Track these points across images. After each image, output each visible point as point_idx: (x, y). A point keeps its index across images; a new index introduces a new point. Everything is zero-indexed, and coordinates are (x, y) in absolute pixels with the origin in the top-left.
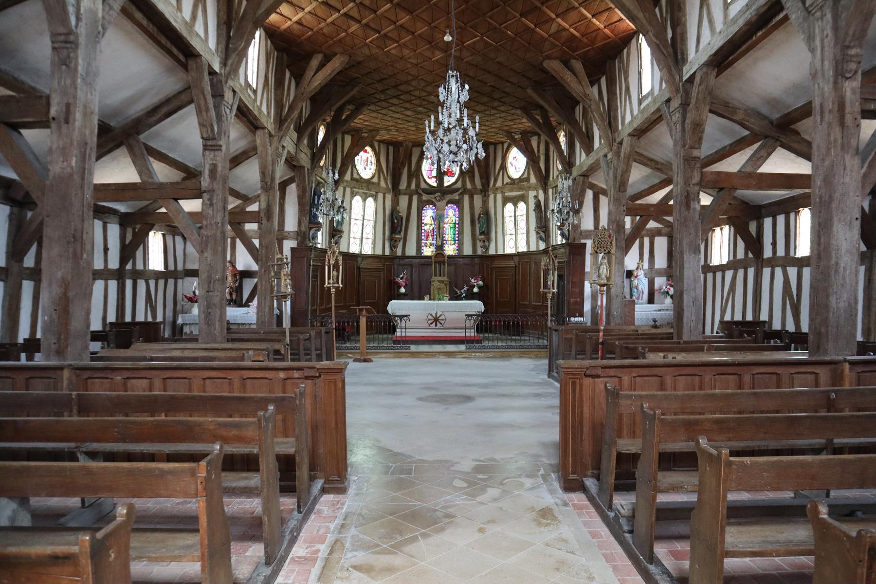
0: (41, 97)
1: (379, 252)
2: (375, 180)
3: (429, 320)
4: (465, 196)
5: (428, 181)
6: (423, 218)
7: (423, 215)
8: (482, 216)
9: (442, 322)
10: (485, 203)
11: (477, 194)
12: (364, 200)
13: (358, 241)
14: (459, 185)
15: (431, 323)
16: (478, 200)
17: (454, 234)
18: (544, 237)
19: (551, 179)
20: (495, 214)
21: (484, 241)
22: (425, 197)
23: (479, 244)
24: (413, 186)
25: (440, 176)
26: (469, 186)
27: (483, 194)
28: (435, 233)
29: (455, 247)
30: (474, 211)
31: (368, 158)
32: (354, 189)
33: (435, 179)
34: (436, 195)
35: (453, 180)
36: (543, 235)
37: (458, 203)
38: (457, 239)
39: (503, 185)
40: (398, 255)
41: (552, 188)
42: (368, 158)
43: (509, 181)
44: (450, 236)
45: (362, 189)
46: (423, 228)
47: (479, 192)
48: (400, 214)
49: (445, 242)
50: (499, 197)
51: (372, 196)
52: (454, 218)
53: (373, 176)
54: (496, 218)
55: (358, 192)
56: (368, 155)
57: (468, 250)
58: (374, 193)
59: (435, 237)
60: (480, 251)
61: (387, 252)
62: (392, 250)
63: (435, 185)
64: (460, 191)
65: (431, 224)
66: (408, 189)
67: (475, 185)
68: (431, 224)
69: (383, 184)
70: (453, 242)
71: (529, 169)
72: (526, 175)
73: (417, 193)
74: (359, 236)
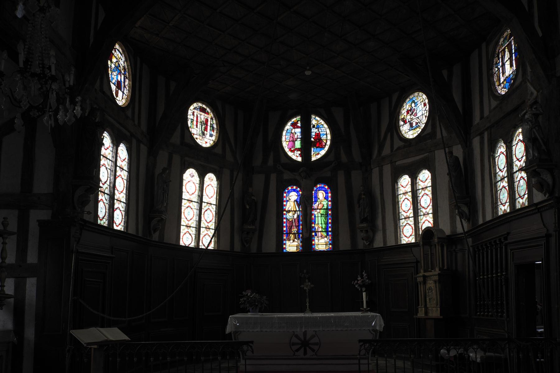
2: (219, 150)
3: (294, 344)
5: (290, 154)
6: (285, 203)
7: (285, 199)
8: (363, 196)
9: (316, 347)
12: (202, 177)
13: (193, 231)
15: (298, 350)
16: (357, 177)
19: (477, 119)
20: (382, 193)
22: (287, 176)
23: (360, 235)
24: (271, 162)
25: (305, 151)
26: (344, 158)
28: (301, 223)
33: (299, 152)
34: (301, 170)
35: (323, 152)
36: (465, 209)
39: (392, 151)
41: (481, 134)
42: (207, 120)
43: (401, 144)
46: (285, 216)
48: (253, 197)
50: (387, 169)
57: (345, 244)
59: (301, 227)
60: (361, 244)
61: (238, 247)
63: (299, 159)
65: (295, 211)
70: (325, 234)
74: (193, 224)
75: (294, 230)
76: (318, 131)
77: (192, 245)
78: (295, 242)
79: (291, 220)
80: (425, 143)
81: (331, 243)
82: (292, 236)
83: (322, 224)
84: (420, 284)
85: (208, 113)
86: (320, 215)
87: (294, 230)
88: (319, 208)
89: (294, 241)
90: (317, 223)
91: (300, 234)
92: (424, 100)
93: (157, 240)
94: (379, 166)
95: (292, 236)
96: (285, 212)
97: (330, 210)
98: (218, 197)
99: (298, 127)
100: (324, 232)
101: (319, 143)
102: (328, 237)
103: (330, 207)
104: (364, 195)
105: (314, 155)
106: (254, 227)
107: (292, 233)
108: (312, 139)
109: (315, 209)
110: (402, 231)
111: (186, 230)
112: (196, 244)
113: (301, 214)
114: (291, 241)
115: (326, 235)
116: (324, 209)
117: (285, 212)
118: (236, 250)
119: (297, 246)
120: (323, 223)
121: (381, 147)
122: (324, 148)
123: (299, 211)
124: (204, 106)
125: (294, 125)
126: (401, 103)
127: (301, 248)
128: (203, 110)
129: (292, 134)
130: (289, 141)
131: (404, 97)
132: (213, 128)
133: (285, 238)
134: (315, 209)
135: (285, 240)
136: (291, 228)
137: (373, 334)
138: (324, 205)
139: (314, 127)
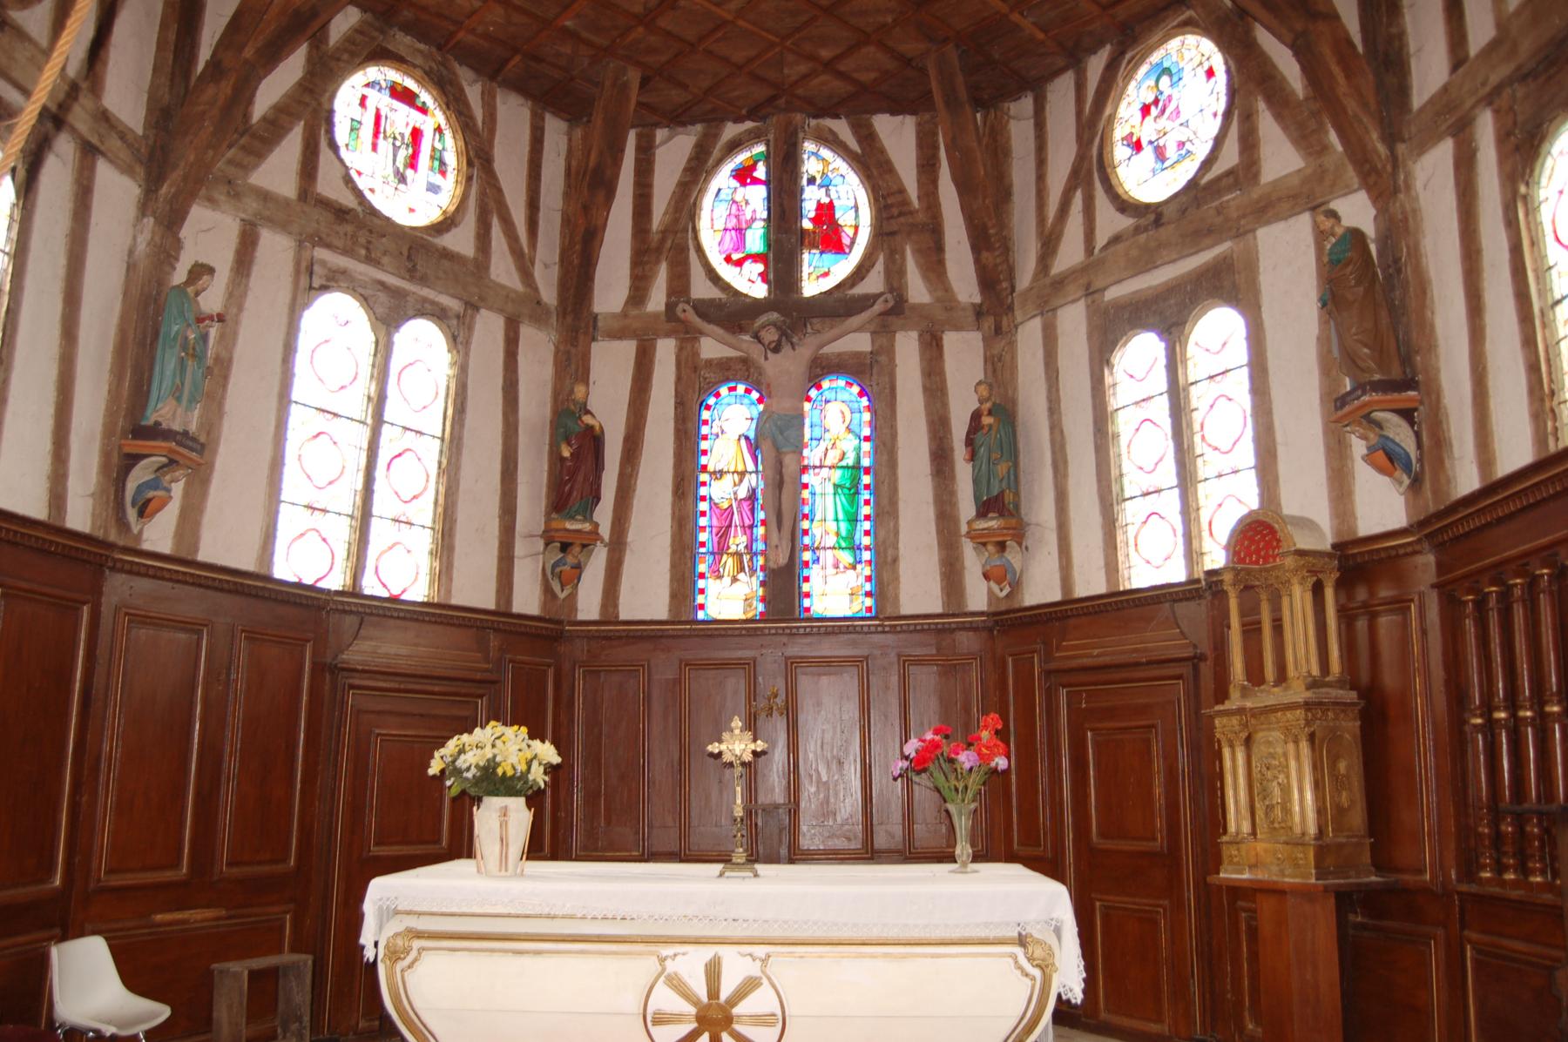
0: (731, 764)
1: (474, 590)
3: (661, 1019)
4: (900, 337)
5: (727, 273)
10: (999, 369)
11: (958, 328)
12: (387, 319)
14: (874, 283)
17: (854, 520)
18: (1409, 445)
21: (1002, 546)
22: (712, 348)
23: (973, 562)
24: (657, 300)
26: (918, 290)
27: (989, 322)
28: (761, 515)
29: (857, 579)
30: (945, 405)
31: (416, 134)
32: (321, 253)
33: (760, 267)
34: (763, 319)
35: (842, 267)
37: (861, 370)
38: (866, 541)
40: (581, 616)
42: (416, 134)
43: (1125, 222)
44: (832, 526)
45: (376, 263)
47: (971, 318)
49: (807, 556)
50: (1073, 319)
51: (438, 315)
52: (849, 444)
53: (447, 224)
54: (1056, 428)
55: (344, 272)
56: (427, 124)
58: (453, 304)
59: (760, 531)
62: (554, 596)
63: (760, 291)
64: (878, 307)
65: (742, 474)
66: (634, 312)
67: (947, 289)
68: (742, 474)
69: (503, 270)
70: (846, 557)
71: (1248, 119)
72: (1231, 157)
73: (672, 321)
74: (345, 497)
75: (737, 542)
76: (828, 195)
77: (335, 582)
78: (738, 583)
79: (725, 505)
80: (1216, 203)
81: (1000, 730)
82: (729, 563)
83: (837, 520)
84: (1232, 746)
85: (423, 110)
86: (830, 489)
87: (738, 541)
88: (828, 462)
89: (735, 580)
90: (818, 516)
91: (756, 554)
92: (1204, 58)
93: (165, 547)
94: (1042, 314)
95: (729, 563)
96: (704, 477)
97: (867, 471)
98: (450, 412)
99: (756, 181)
100: (846, 548)
101: (830, 238)
102: (859, 567)
103: (866, 462)
104: (990, 413)
105: (814, 276)
106: (587, 527)
107: (730, 551)
108: (807, 225)
109: (815, 467)
110: (1132, 543)
111: (305, 519)
112: (348, 578)
113: (761, 485)
114: (727, 580)
115: (851, 560)
116: (847, 467)
117: (704, 477)
118: (517, 608)
119: (746, 600)
120: (841, 516)
121: (1049, 243)
122: (849, 254)
123: (757, 472)
124: (410, 84)
125: (744, 176)
126: (1121, 84)
127: (761, 607)
128: (403, 95)
129: (734, 207)
130: (726, 230)
131: (1129, 62)
132: (442, 163)
133: (702, 568)
134: (815, 467)
135: (702, 576)
136: (723, 534)
137: (1033, 979)
138: (844, 454)
139: (812, 181)
